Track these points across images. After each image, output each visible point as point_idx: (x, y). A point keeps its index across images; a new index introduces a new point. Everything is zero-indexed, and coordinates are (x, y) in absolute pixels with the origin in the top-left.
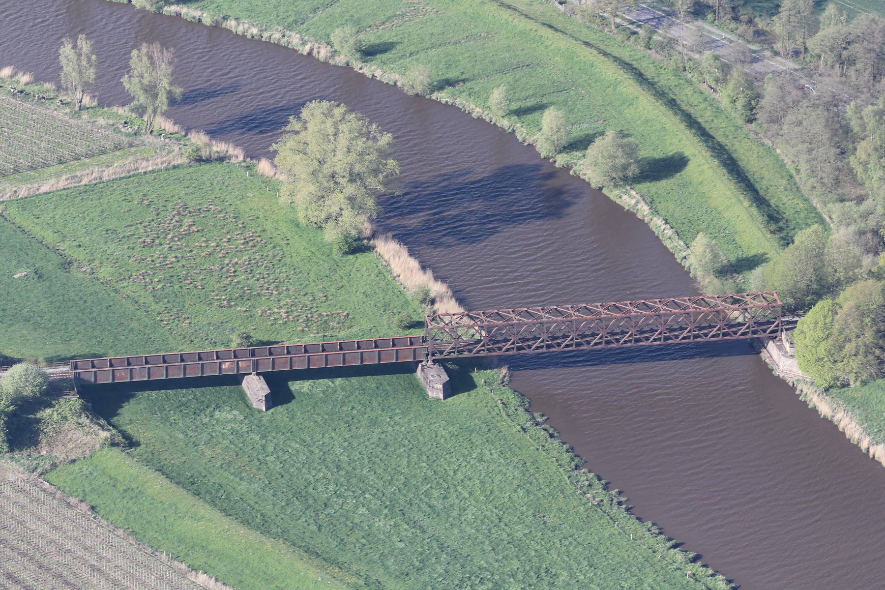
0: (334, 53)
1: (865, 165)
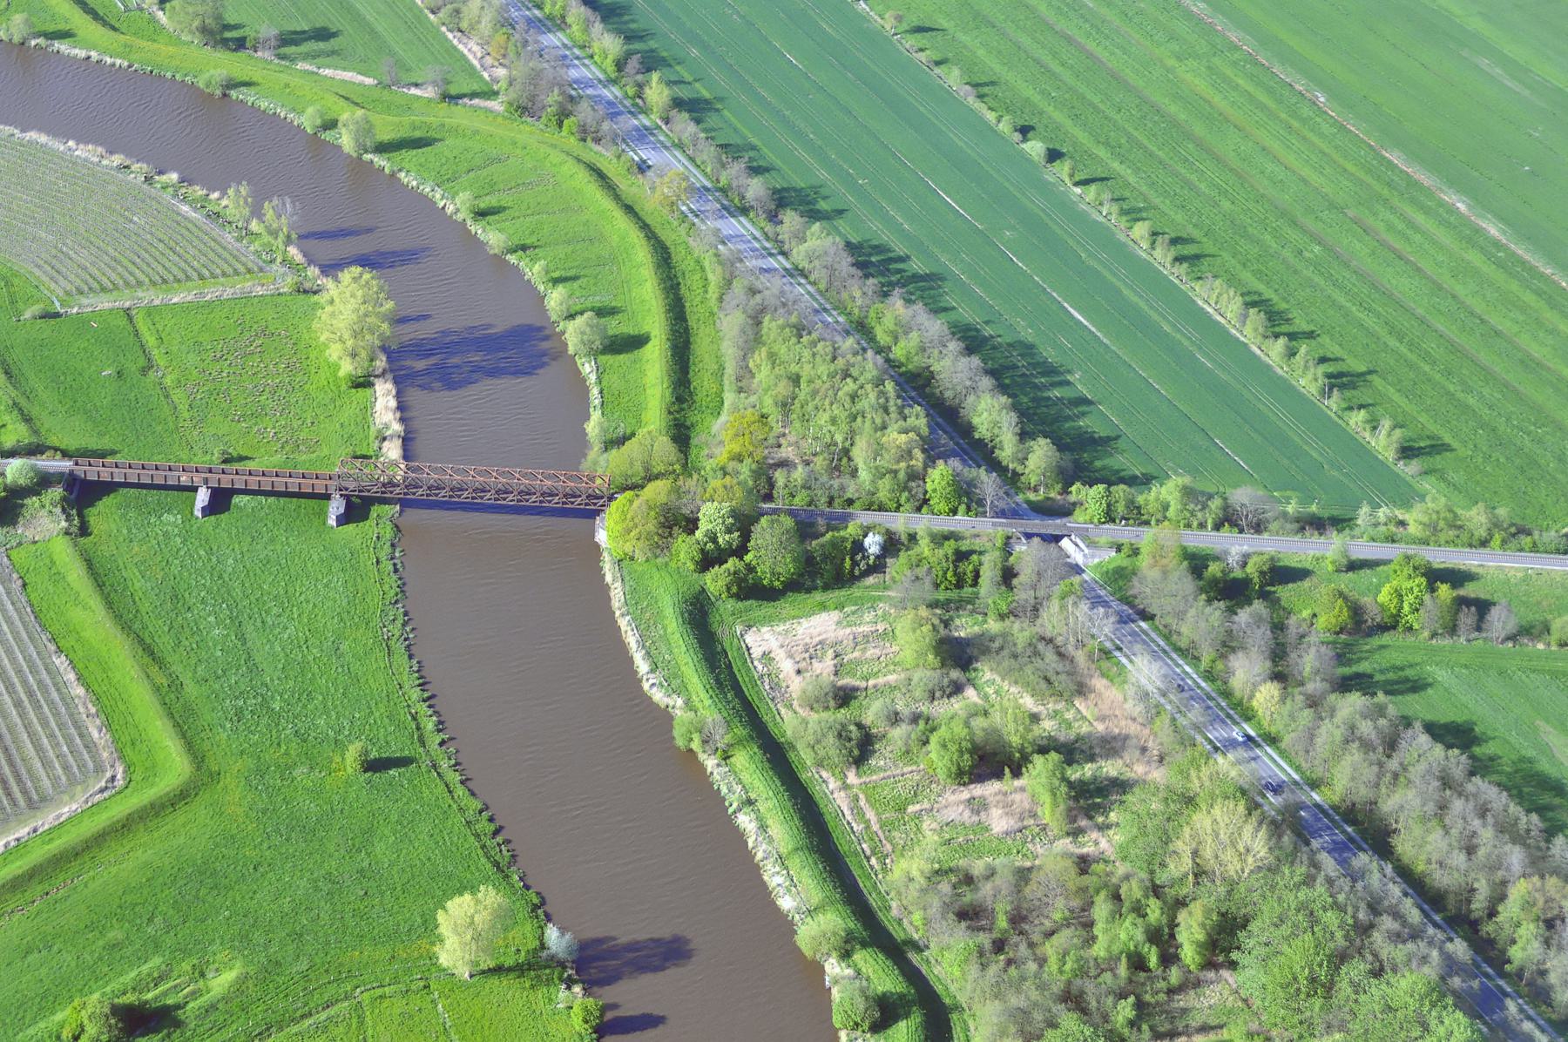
0: (458, 210)
1: (759, 366)
